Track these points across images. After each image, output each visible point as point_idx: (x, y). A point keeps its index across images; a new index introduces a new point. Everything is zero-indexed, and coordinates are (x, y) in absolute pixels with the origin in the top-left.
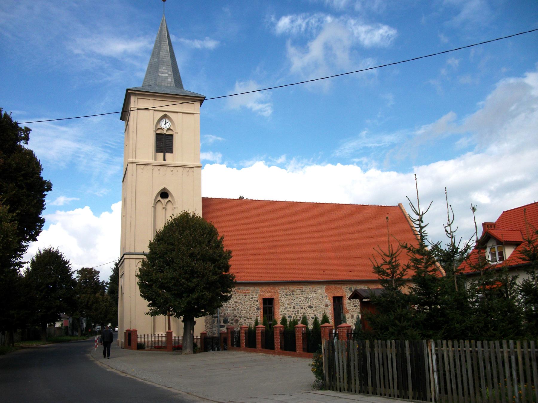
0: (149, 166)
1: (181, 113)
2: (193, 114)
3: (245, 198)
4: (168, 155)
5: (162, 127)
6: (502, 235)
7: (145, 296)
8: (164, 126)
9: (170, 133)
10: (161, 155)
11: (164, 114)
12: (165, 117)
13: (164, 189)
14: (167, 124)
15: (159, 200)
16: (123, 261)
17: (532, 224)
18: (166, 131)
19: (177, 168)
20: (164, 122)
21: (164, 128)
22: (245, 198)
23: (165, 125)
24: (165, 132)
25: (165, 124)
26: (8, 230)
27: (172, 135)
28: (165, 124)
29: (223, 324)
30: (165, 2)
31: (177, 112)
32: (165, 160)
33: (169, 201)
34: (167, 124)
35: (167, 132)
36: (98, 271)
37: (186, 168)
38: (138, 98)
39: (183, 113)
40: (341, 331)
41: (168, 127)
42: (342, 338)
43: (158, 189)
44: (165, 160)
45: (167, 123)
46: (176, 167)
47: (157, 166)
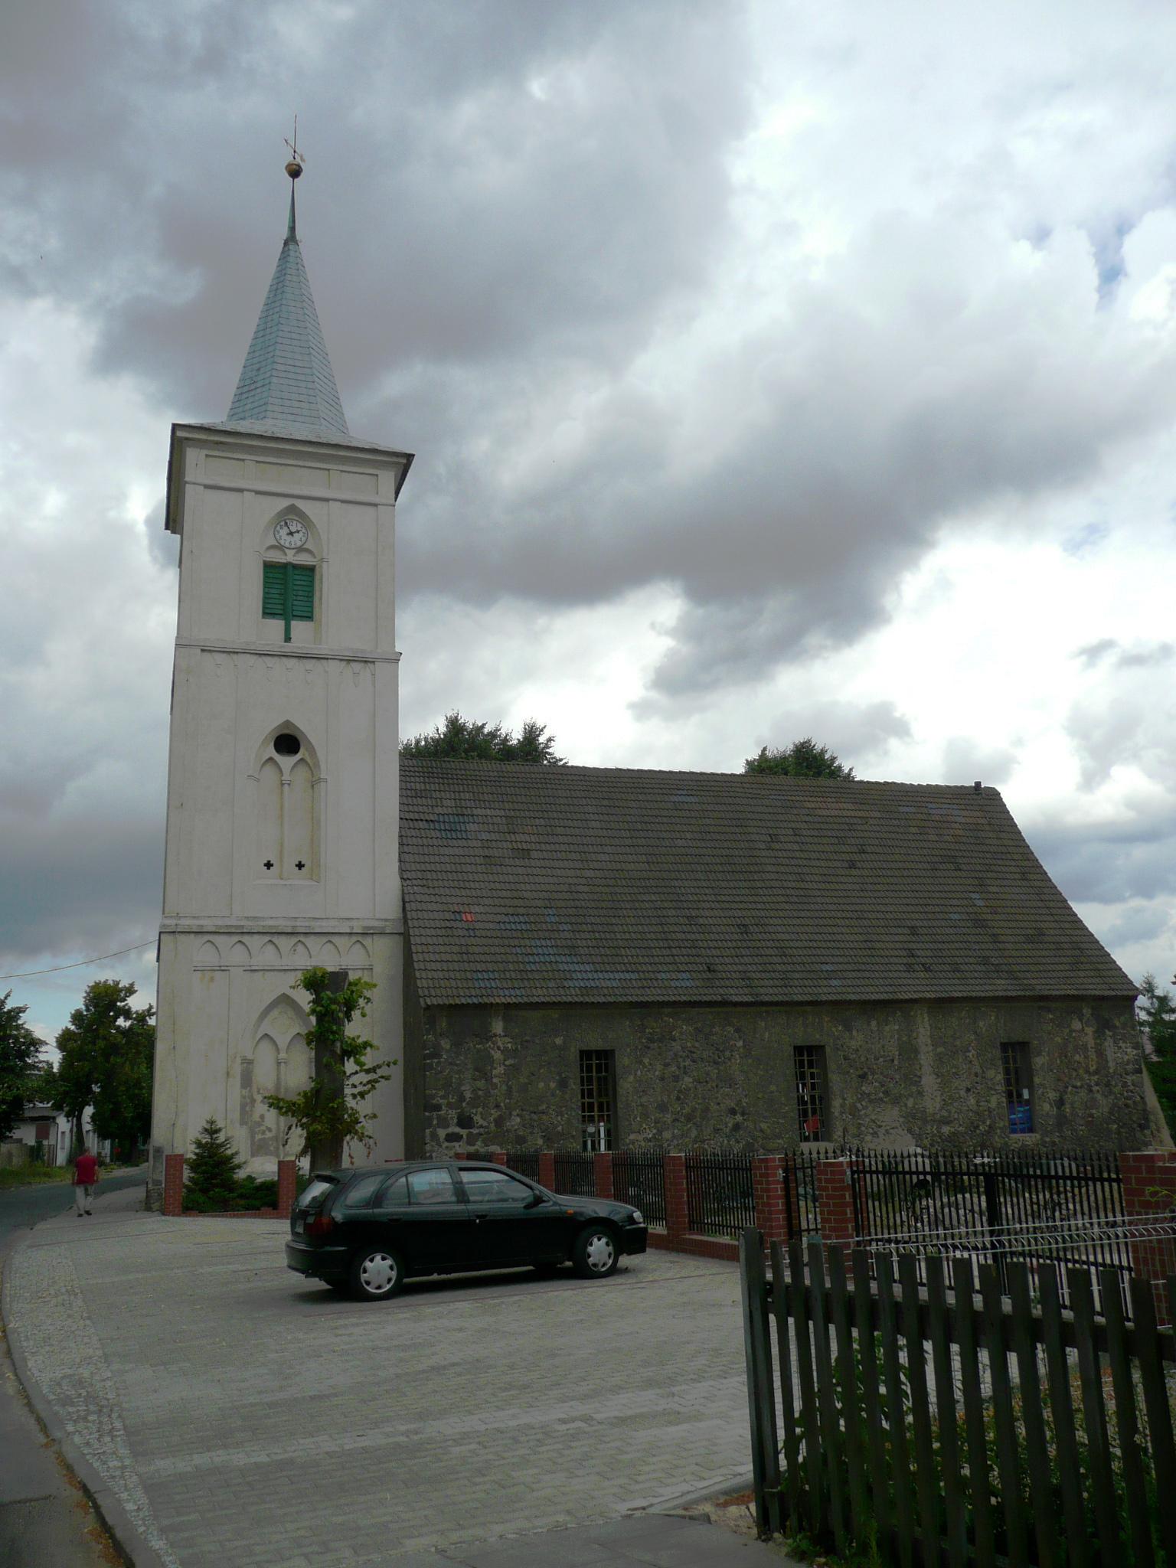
1: (253, 493)
2: (376, 505)
4: (297, 626)
5: (282, 542)
6: (292, 1483)
9: (304, 559)
10: (277, 625)
11: (285, 506)
13: (287, 723)
15: (271, 759)
17: (498, 1460)
21: (287, 545)
27: (311, 570)
29: (457, 1130)
30: (296, 180)
31: (241, 490)
32: (288, 639)
33: (302, 759)
35: (295, 558)
36: (976, 783)
38: (207, 456)
39: (258, 493)
40: (762, 1184)
41: (299, 544)
42: (767, 1199)
43: (270, 724)
44: (288, 639)
46: (322, 661)
47: (264, 658)
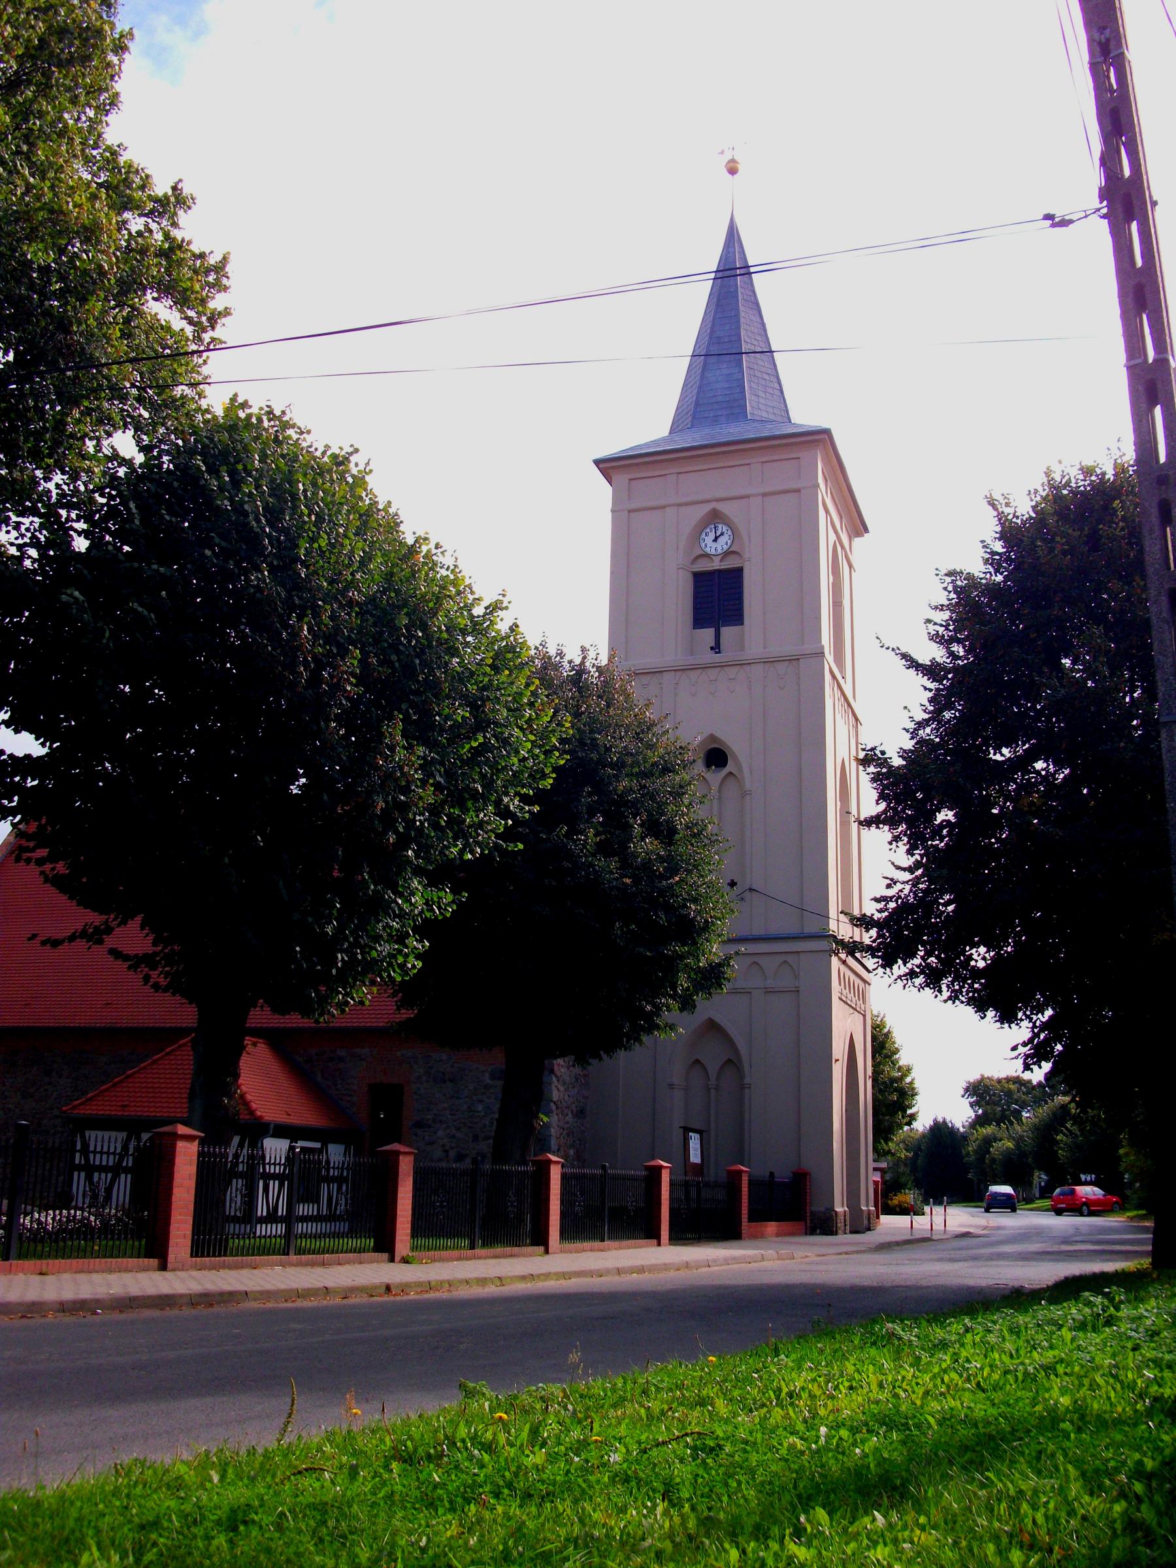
0: (665, 674)
3: (33, 736)
4: (727, 632)
5: (708, 550)
7: (25, 755)
8: (714, 545)
10: (708, 634)
12: (714, 518)
14: (719, 540)
16: (1066, 1241)
18: (721, 561)
19: (747, 668)
20: (712, 536)
21: (713, 552)
22: (33, 736)
23: (714, 545)
24: (716, 565)
25: (715, 540)
26: (339, 1439)
27: (740, 571)
28: (715, 540)
33: (731, 773)
34: (722, 540)
37: (709, 671)
45: (722, 534)
